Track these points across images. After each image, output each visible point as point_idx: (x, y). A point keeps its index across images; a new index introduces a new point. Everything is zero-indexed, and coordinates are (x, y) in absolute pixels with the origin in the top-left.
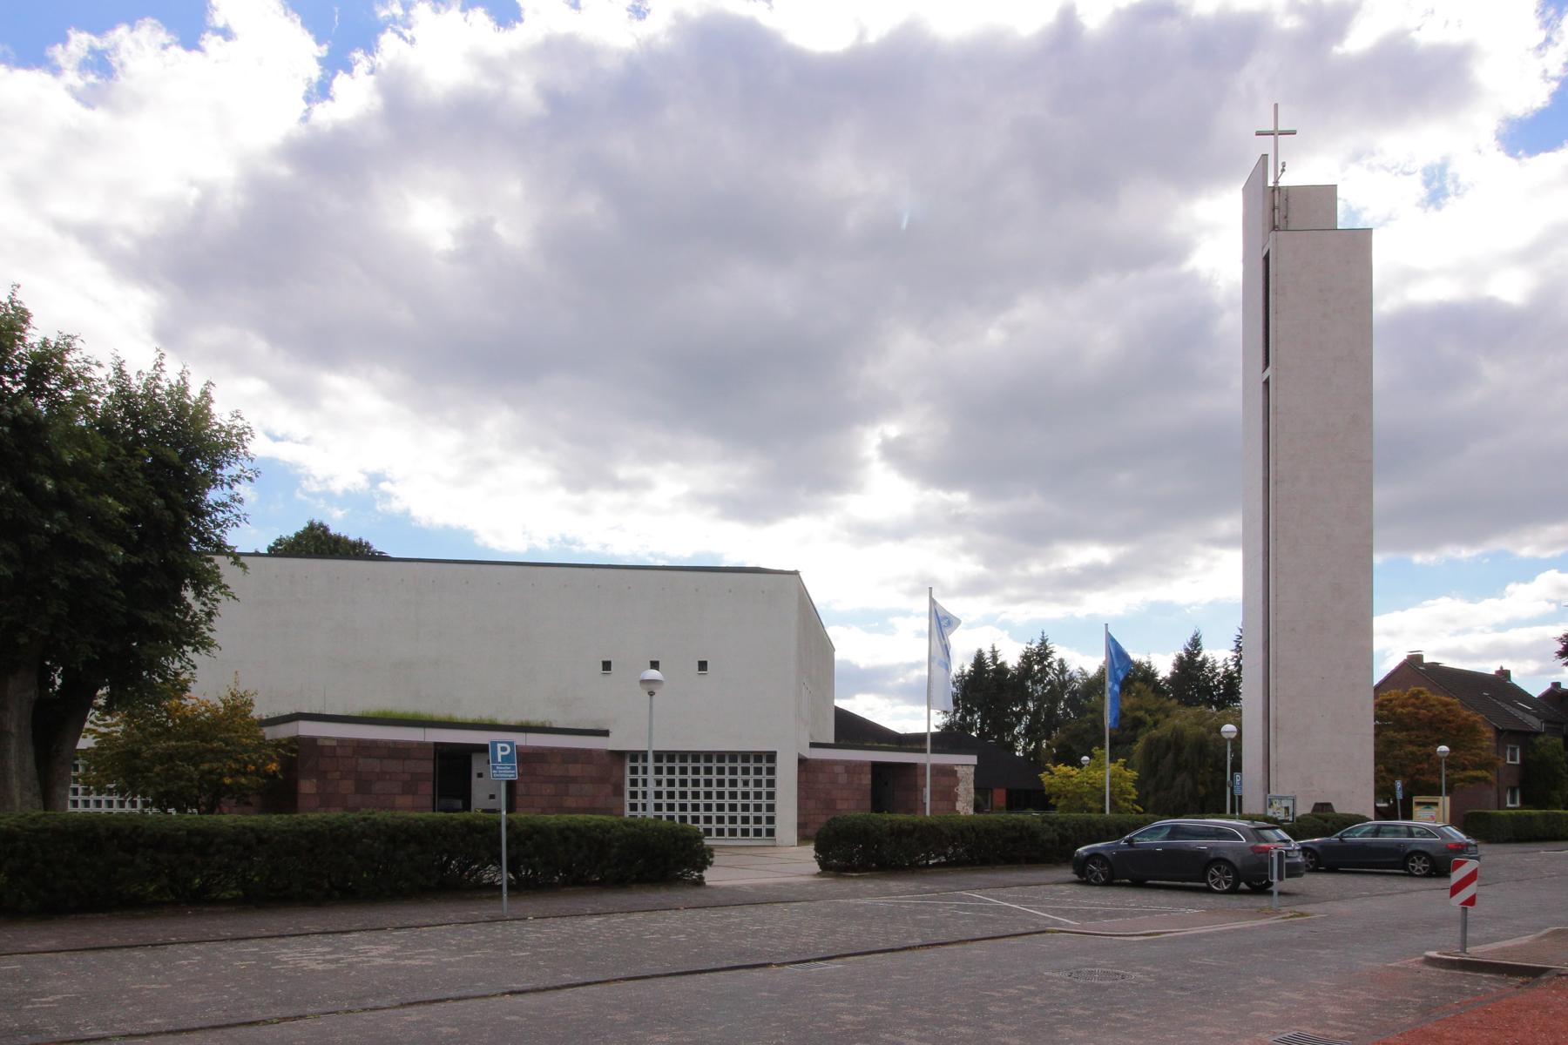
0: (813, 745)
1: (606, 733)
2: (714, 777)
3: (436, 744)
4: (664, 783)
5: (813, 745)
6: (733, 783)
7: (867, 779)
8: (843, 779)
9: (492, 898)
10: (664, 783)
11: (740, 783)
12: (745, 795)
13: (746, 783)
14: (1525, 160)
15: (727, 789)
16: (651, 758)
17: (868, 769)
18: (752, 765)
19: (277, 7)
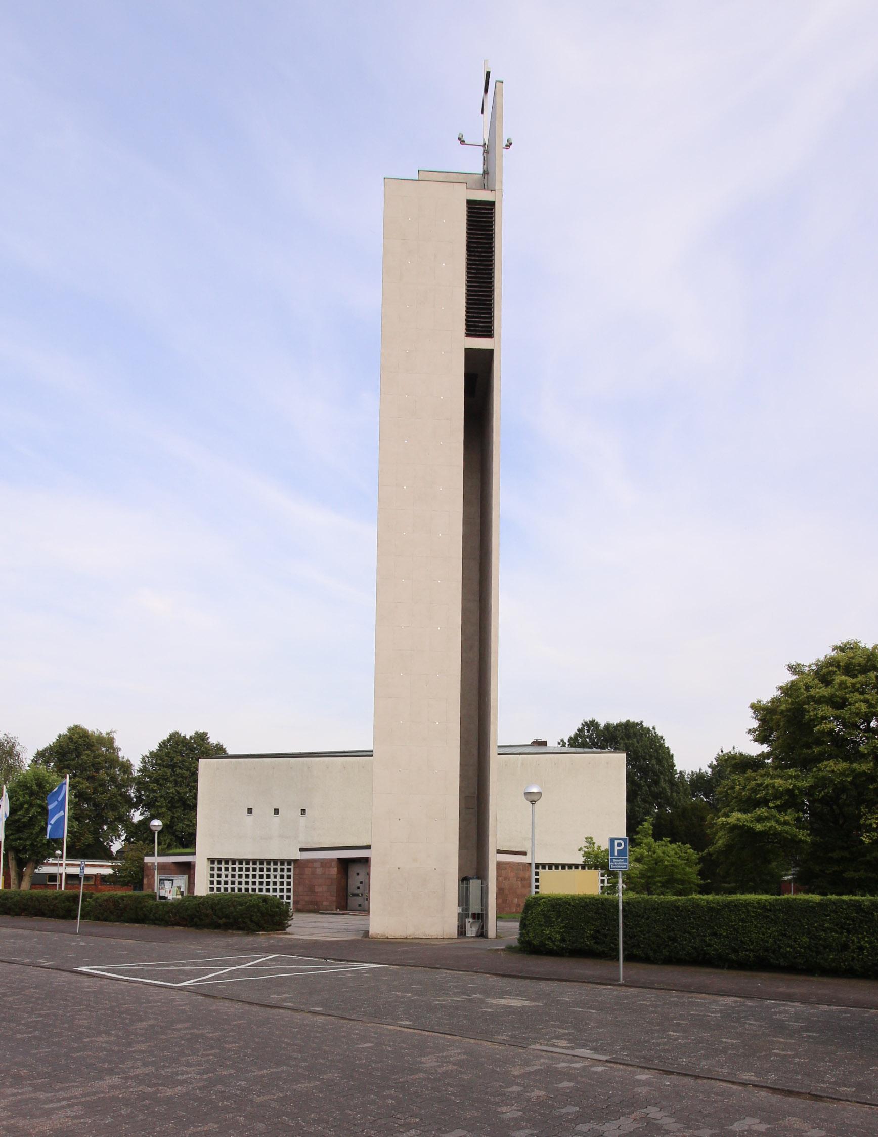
0: (302, 850)
1: (525, 854)
2: (251, 873)
3: (339, 859)
4: (230, 876)
5: (302, 850)
6: (268, 877)
7: (334, 871)
8: (319, 871)
9: (610, 963)
10: (230, 876)
11: (272, 877)
12: (275, 883)
13: (275, 877)
14: (788, 678)
15: (265, 880)
16: (533, 866)
17: (334, 864)
18: (279, 867)
19: (877, 634)
